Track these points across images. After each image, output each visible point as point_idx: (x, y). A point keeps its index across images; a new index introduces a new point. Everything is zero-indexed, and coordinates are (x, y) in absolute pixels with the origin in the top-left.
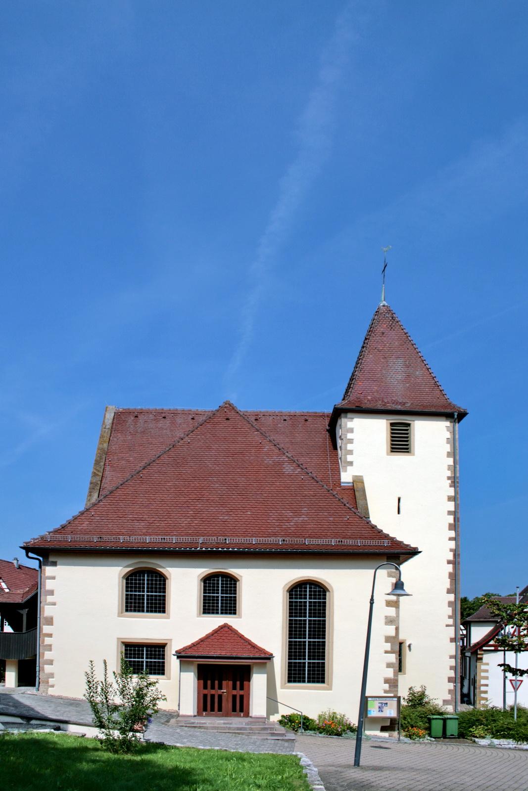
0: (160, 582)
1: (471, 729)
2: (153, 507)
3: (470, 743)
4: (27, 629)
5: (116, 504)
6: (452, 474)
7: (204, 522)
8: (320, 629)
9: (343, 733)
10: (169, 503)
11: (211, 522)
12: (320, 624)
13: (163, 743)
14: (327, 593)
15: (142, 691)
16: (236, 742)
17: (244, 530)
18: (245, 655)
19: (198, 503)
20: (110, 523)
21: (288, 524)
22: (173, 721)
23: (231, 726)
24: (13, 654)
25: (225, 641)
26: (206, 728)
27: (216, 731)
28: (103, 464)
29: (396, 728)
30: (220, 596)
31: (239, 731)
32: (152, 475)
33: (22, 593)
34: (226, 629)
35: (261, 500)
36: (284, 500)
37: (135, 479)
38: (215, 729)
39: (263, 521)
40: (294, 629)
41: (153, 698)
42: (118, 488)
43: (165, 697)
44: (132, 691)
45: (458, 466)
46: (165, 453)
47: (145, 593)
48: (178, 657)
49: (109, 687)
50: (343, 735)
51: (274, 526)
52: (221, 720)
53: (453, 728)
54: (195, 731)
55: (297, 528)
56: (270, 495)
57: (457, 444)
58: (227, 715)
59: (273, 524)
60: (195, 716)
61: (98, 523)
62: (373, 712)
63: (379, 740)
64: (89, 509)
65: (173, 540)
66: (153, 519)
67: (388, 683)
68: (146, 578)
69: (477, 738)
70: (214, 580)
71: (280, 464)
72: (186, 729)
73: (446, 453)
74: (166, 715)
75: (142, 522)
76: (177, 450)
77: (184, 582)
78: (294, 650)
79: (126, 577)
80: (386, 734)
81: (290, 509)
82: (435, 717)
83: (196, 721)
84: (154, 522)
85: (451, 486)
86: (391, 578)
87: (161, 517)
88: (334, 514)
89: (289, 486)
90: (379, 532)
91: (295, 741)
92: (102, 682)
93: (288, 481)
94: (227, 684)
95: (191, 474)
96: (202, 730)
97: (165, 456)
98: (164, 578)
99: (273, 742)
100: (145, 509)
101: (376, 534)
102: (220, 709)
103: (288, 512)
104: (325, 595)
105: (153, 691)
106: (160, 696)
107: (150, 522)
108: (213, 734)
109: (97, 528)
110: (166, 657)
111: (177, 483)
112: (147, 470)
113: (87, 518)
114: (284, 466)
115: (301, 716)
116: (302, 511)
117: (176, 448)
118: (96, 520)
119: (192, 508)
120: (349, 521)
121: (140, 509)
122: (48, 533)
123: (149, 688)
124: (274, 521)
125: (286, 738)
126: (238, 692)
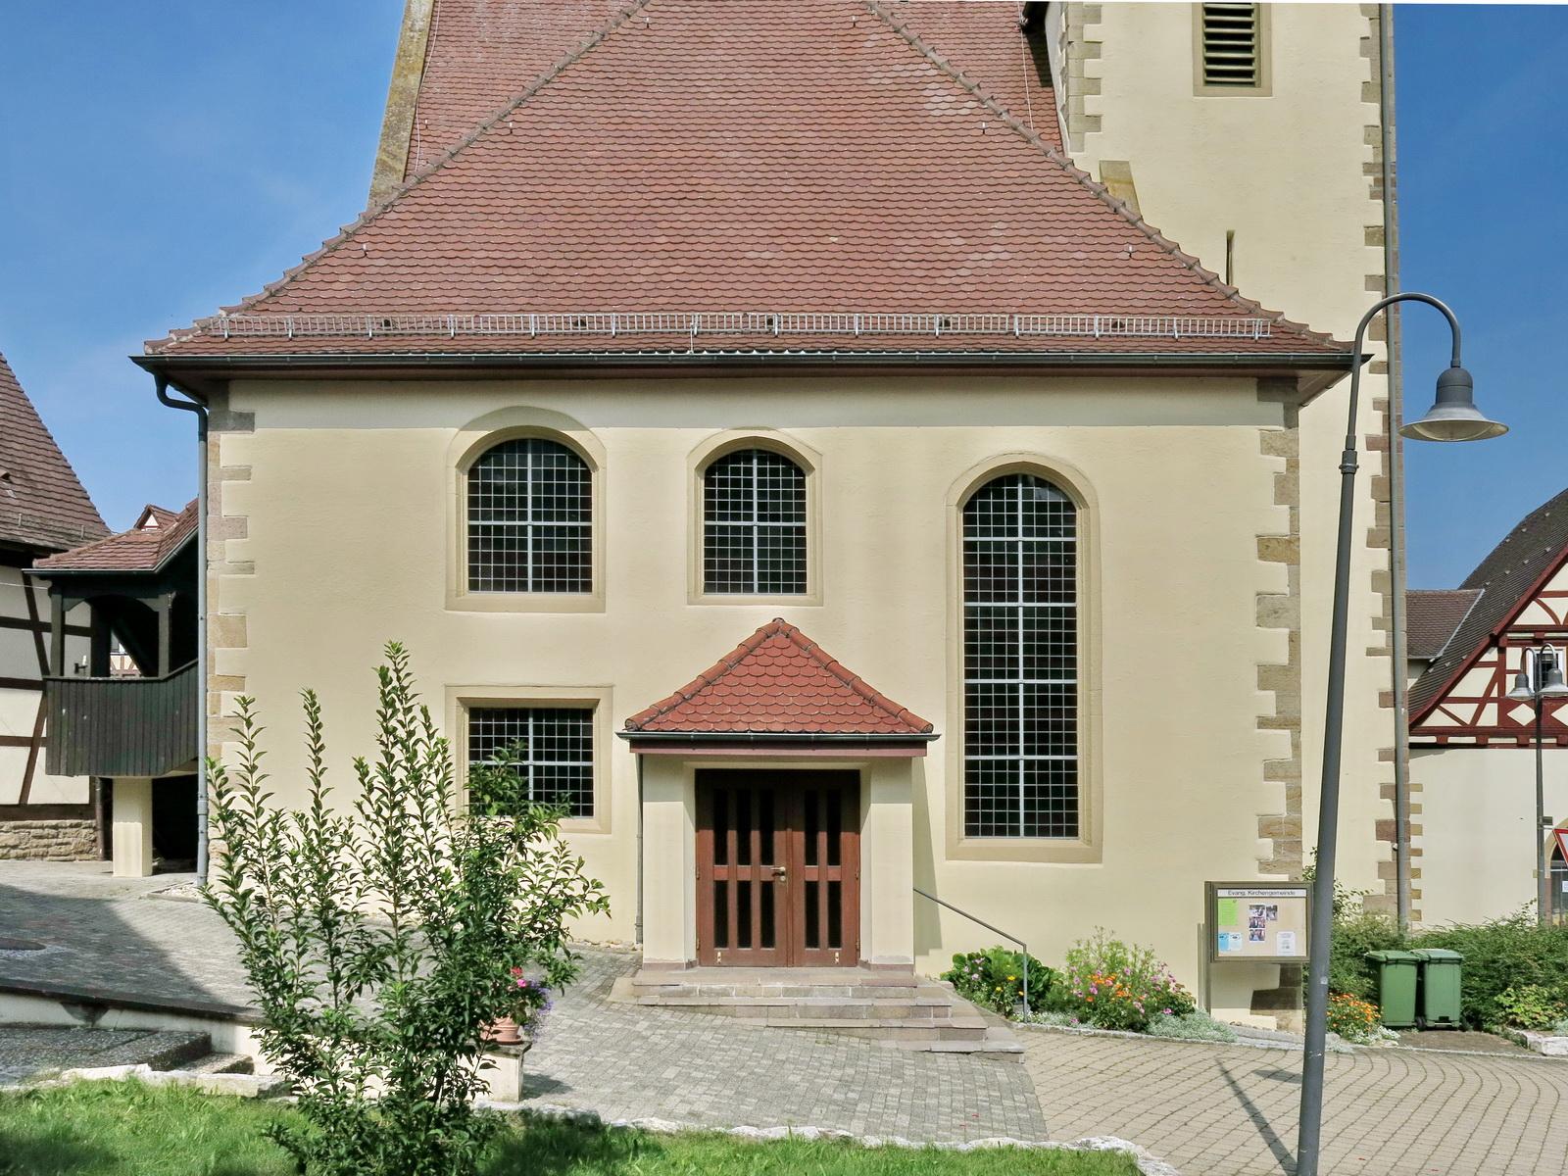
0: (568, 476)
1: (1500, 998)
2: (547, 225)
3: (1507, 1049)
4: (172, 666)
5: (437, 216)
6: (1375, 155)
7: (703, 270)
8: (1057, 644)
9: (1152, 1019)
10: (595, 210)
11: (723, 270)
12: (986, 662)
13: (596, 1119)
14: (1079, 513)
15: (494, 864)
16: (838, 1073)
17: (825, 294)
18: (847, 732)
19: (682, 210)
20: (418, 278)
21: (953, 273)
22: (622, 984)
23: (810, 1001)
24: (132, 755)
25: (779, 681)
26: (729, 1011)
27: (763, 1022)
28: (406, 135)
29: (1300, 1000)
30: (755, 519)
31: (834, 1026)
32: (544, 126)
33: (159, 539)
34: (780, 639)
35: (866, 197)
36: (933, 197)
37: (492, 138)
38: (759, 1016)
39: (877, 264)
40: (985, 645)
41: (547, 897)
42: (441, 166)
43: (603, 892)
44: (446, 864)
45: (1392, 129)
46: (579, 57)
47: (531, 525)
48: (636, 743)
49: (337, 841)
50: (1153, 1027)
51: (913, 280)
52: (777, 977)
53: (1446, 993)
54: (697, 1027)
55: (981, 287)
56: (893, 183)
57: (1390, 58)
58: (789, 960)
59: (908, 273)
60: (690, 965)
61: (380, 278)
62: (1236, 944)
63: (1258, 1043)
64: (354, 234)
65: (614, 327)
66: (550, 263)
67: (1271, 834)
68: (530, 468)
69: (1525, 1027)
70: (736, 471)
71: (917, 86)
72: (666, 1015)
73: (1360, 87)
74: (600, 963)
75: (515, 271)
76: (612, 50)
77: (646, 465)
78: (985, 721)
79: (469, 466)
80: (1267, 1021)
81: (956, 226)
82: (1393, 954)
83: (698, 986)
84: (551, 272)
85: (1373, 196)
86: (1272, 457)
87: (573, 255)
88: (1086, 240)
89: (944, 154)
90: (1229, 298)
91: (1021, 1058)
92: (301, 818)
93: (941, 140)
94: (789, 841)
95: (658, 121)
96: (718, 1021)
97: (579, 67)
98: (584, 465)
99: (953, 1062)
100: (524, 232)
101: (1219, 304)
102: (768, 939)
103: (949, 234)
104: (1071, 520)
105: (547, 859)
106: (576, 889)
107: (536, 271)
108: (754, 1037)
109: (378, 293)
110: (595, 750)
111: (616, 147)
112: (529, 111)
113: (349, 262)
114: (925, 93)
115: (1018, 958)
116: (993, 233)
117: (610, 43)
118: (376, 270)
119: (664, 225)
120: (1132, 263)
121: (509, 232)
122: (224, 314)
123: (527, 845)
124: (909, 264)
125: (992, 1046)
126: (822, 873)
